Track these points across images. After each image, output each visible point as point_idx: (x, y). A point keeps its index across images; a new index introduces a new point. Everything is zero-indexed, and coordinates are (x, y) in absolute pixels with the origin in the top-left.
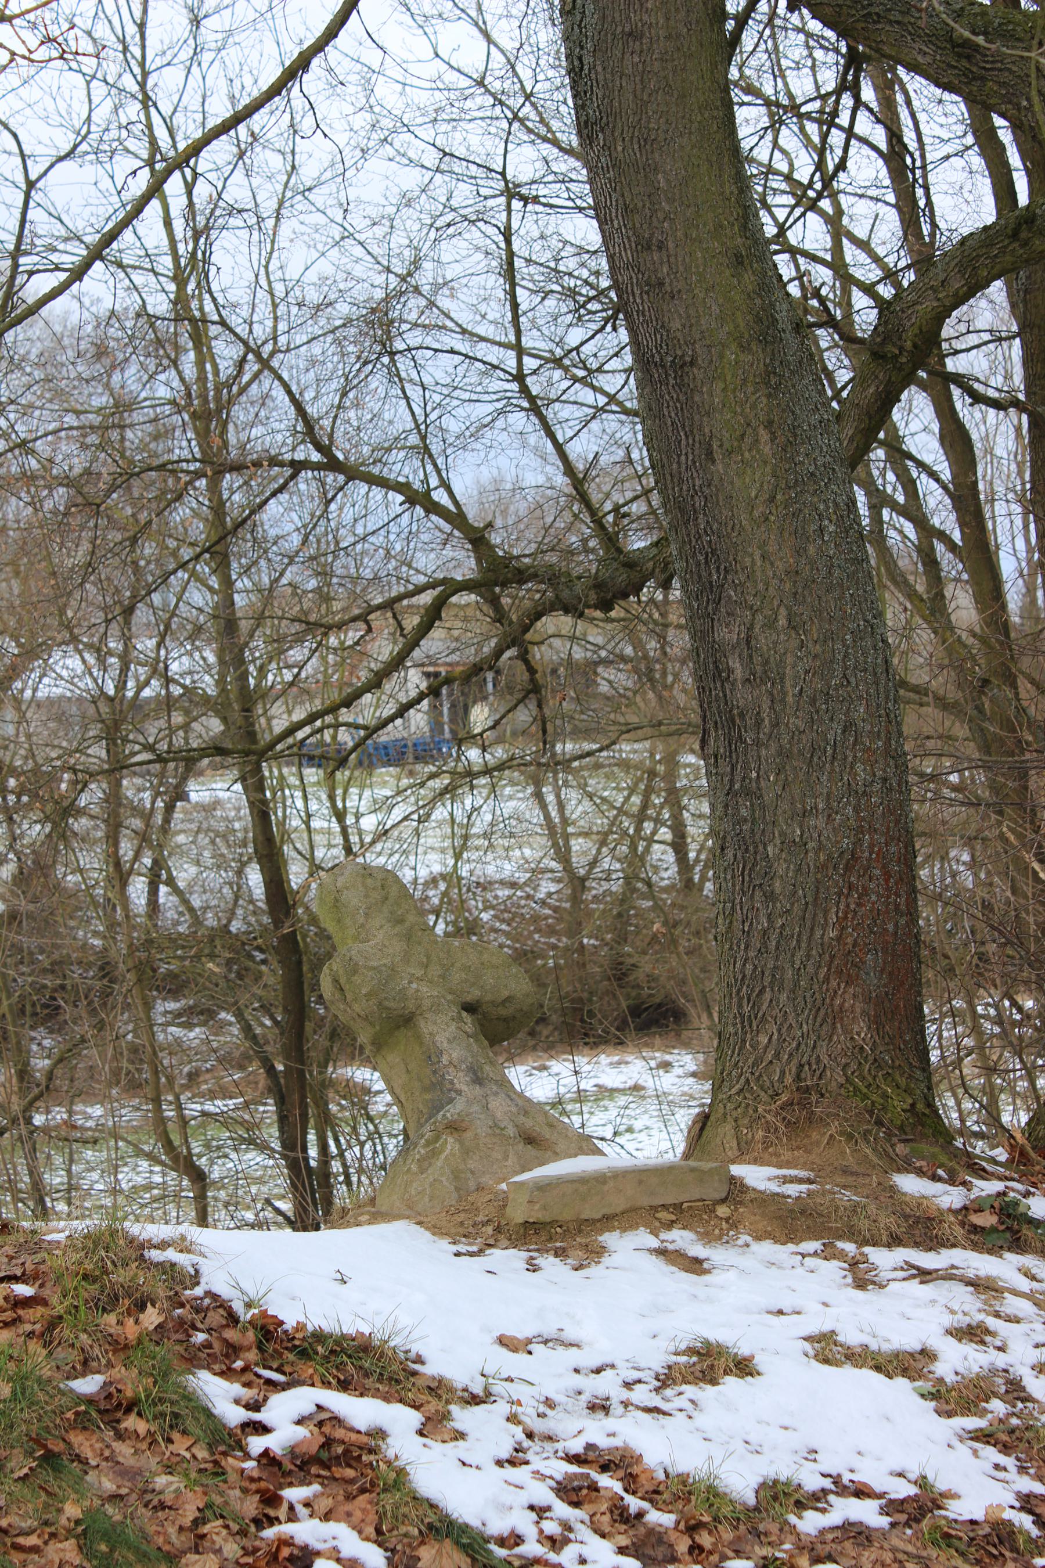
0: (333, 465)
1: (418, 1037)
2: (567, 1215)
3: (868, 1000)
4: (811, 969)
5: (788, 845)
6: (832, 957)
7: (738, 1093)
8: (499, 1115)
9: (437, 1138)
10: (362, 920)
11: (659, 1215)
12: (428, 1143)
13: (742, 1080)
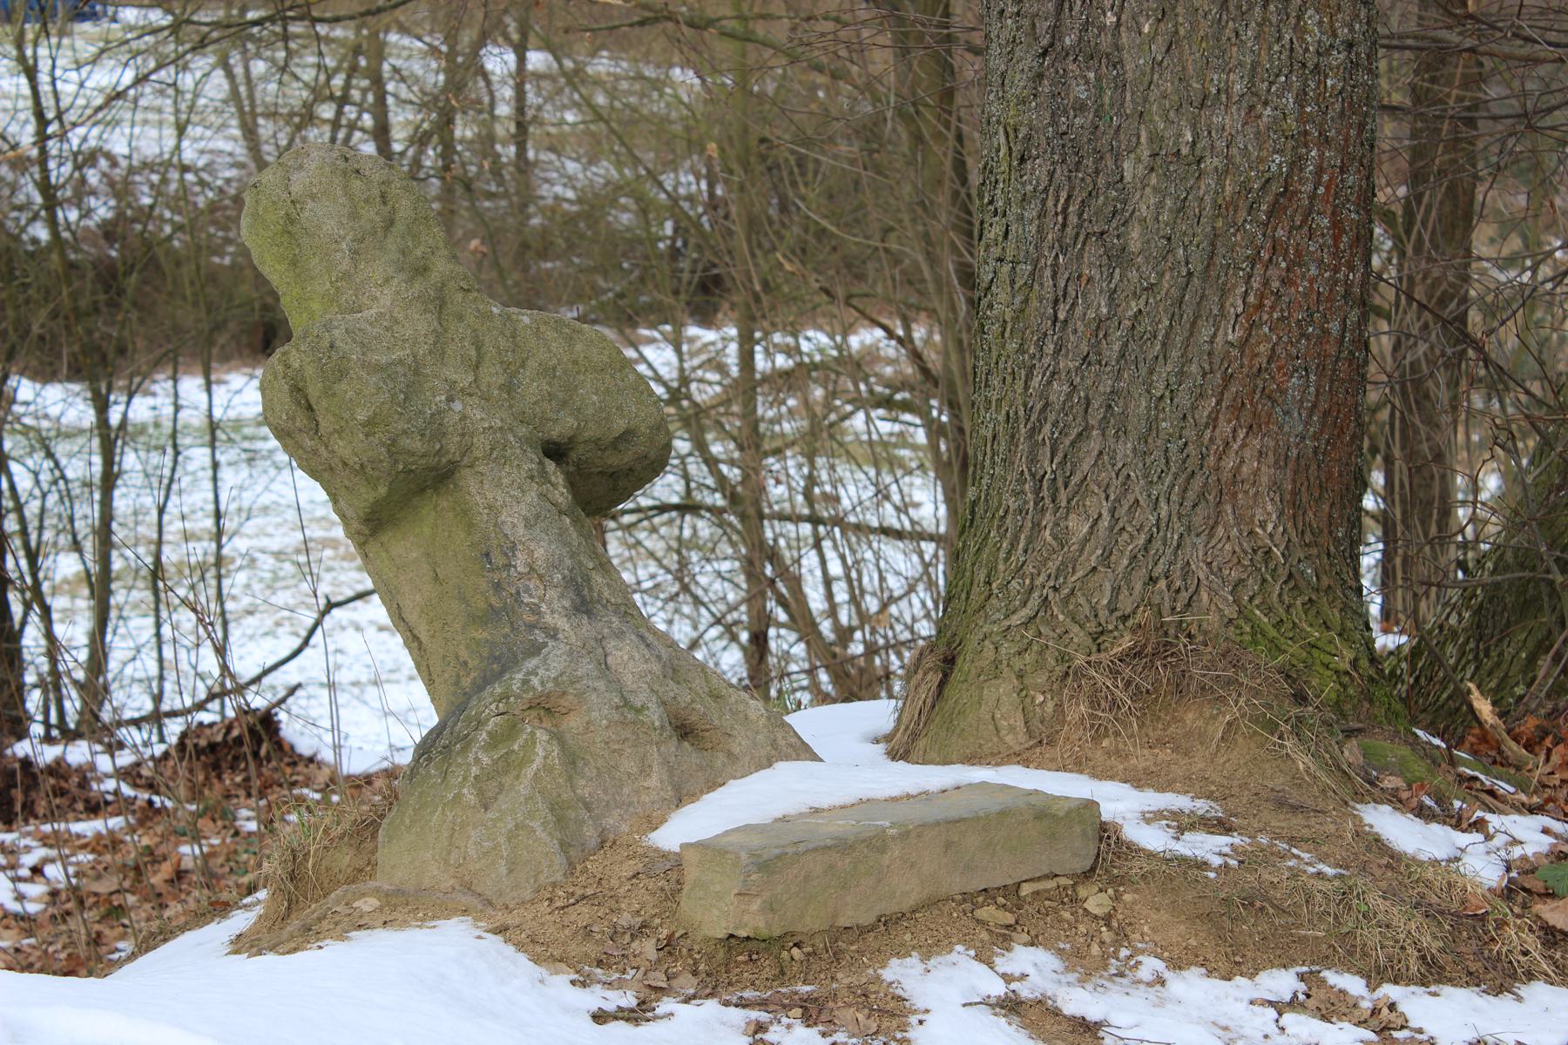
1: (465, 514)
2: (812, 921)
3: (1282, 461)
4: (1184, 400)
5: (1162, 158)
6: (1228, 379)
7: (1025, 625)
8: (628, 679)
9: (512, 730)
10: (345, 265)
11: (982, 913)
12: (495, 741)
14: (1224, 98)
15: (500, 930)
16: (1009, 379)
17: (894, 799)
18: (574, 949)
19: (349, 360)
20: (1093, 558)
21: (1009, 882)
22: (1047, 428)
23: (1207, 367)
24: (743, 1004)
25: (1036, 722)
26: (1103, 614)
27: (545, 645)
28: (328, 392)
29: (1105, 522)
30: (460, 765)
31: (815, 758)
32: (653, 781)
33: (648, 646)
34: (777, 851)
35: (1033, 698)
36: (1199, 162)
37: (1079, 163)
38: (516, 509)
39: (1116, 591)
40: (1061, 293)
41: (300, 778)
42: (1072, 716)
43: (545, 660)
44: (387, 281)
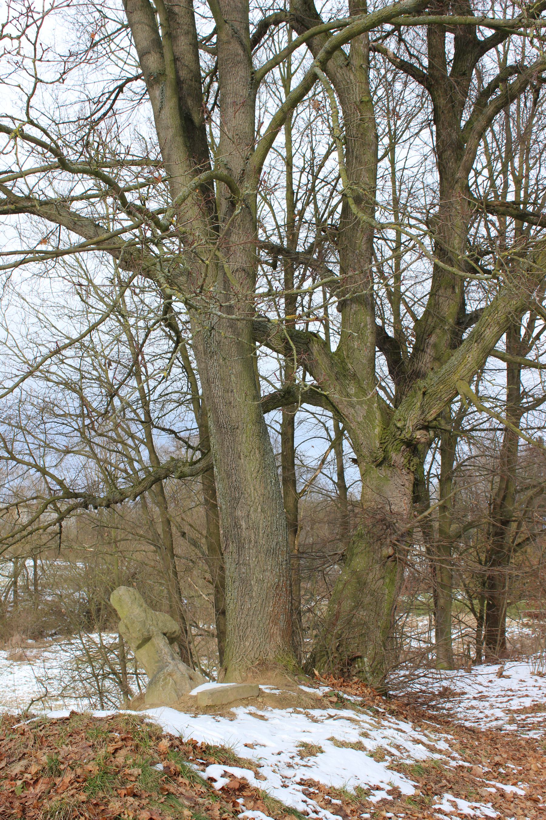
0: (13, 458)
1: (153, 645)
2: (218, 703)
9: (166, 678)
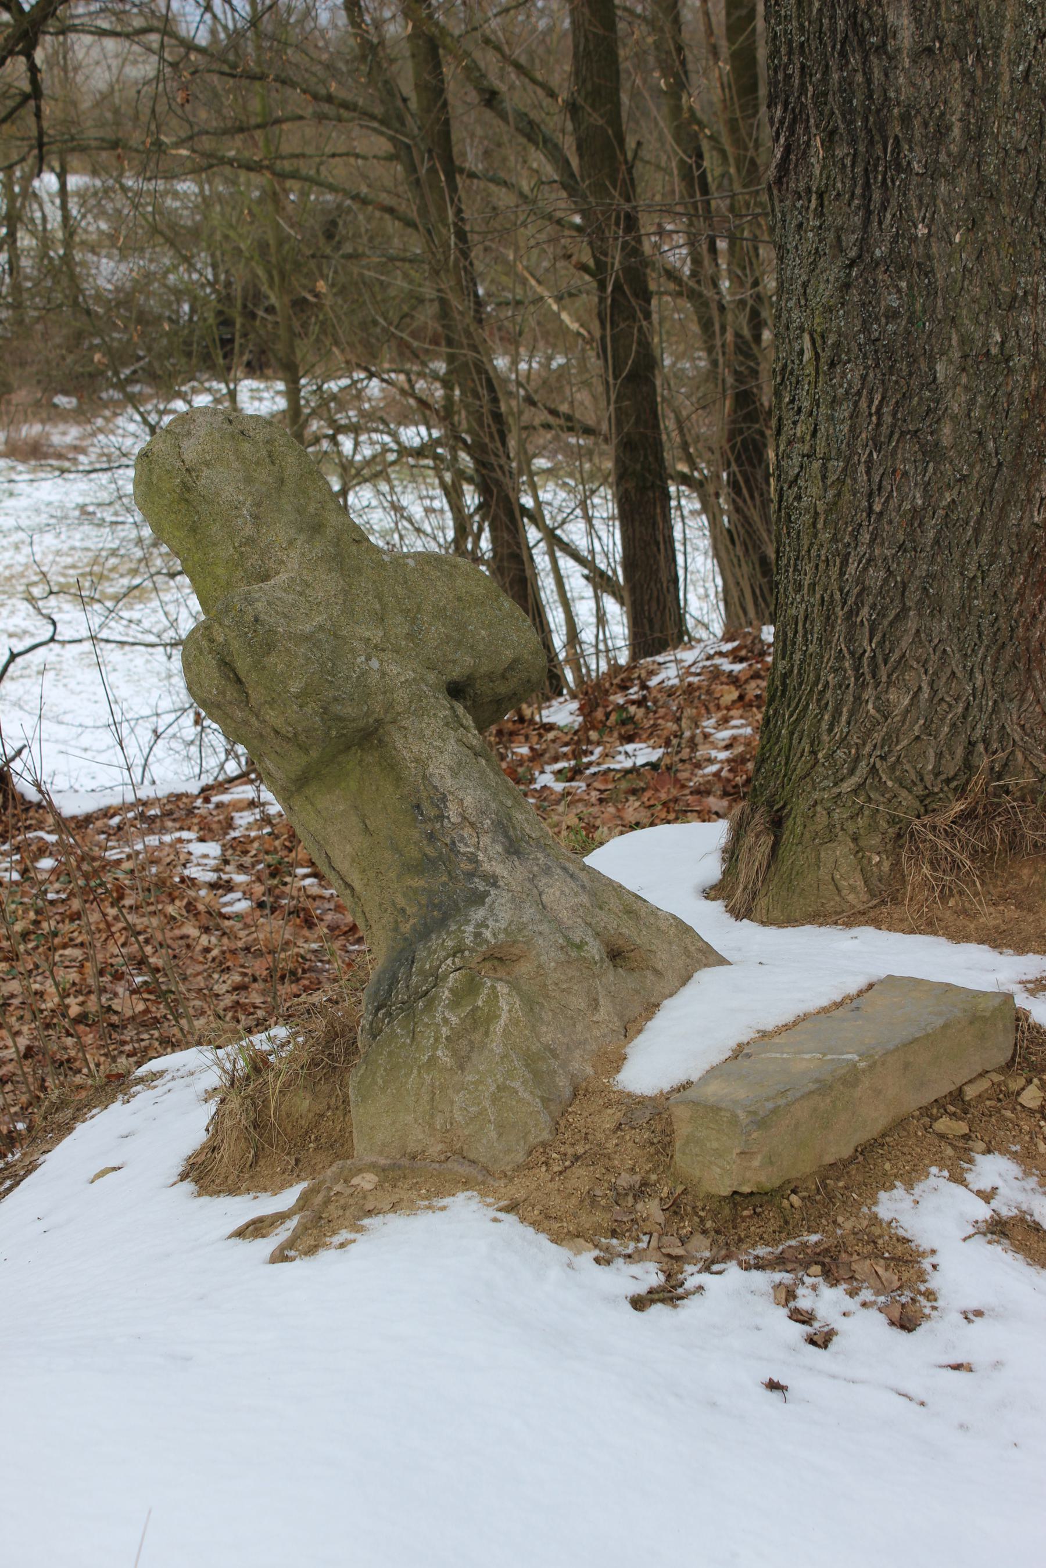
1: (392, 768)
2: (805, 1166)
4: (995, 579)
7: (855, 792)
8: (564, 915)
9: (471, 987)
13: (863, 768)
14: (1030, 299)
15: (511, 1208)
16: (822, 566)
17: (825, 1010)
18: (587, 1221)
19: (276, 633)
20: (916, 728)
21: (953, 1088)
22: (865, 611)
23: (1015, 547)
24: (760, 1265)
25: (874, 881)
26: (929, 778)
27: (487, 894)
28: (258, 666)
29: (925, 694)
30: (427, 1025)
31: (722, 961)
32: (602, 1015)
33: (572, 876)
34: (770, 1105)
35: (870, 859)
36: (1007, 361)
37: (892, 366)
38: (440, 759)
39: (940, 756)
40: (875, 487)
41: (33, 822)
42: (913, 878)
43: (491, 910)
44: (291, 543)
